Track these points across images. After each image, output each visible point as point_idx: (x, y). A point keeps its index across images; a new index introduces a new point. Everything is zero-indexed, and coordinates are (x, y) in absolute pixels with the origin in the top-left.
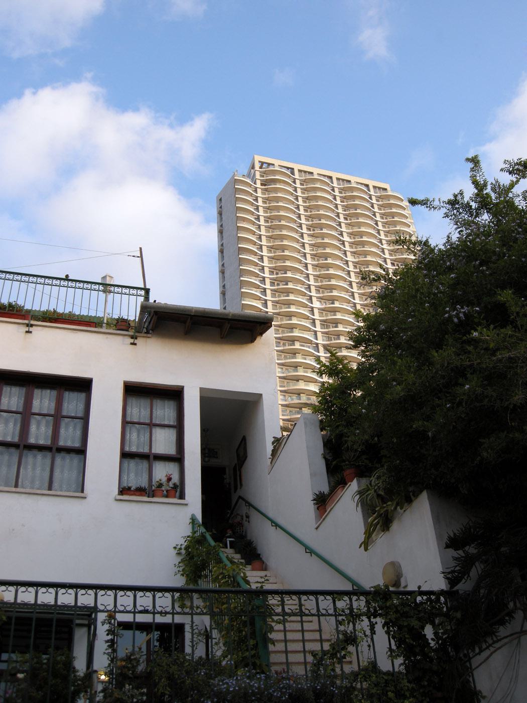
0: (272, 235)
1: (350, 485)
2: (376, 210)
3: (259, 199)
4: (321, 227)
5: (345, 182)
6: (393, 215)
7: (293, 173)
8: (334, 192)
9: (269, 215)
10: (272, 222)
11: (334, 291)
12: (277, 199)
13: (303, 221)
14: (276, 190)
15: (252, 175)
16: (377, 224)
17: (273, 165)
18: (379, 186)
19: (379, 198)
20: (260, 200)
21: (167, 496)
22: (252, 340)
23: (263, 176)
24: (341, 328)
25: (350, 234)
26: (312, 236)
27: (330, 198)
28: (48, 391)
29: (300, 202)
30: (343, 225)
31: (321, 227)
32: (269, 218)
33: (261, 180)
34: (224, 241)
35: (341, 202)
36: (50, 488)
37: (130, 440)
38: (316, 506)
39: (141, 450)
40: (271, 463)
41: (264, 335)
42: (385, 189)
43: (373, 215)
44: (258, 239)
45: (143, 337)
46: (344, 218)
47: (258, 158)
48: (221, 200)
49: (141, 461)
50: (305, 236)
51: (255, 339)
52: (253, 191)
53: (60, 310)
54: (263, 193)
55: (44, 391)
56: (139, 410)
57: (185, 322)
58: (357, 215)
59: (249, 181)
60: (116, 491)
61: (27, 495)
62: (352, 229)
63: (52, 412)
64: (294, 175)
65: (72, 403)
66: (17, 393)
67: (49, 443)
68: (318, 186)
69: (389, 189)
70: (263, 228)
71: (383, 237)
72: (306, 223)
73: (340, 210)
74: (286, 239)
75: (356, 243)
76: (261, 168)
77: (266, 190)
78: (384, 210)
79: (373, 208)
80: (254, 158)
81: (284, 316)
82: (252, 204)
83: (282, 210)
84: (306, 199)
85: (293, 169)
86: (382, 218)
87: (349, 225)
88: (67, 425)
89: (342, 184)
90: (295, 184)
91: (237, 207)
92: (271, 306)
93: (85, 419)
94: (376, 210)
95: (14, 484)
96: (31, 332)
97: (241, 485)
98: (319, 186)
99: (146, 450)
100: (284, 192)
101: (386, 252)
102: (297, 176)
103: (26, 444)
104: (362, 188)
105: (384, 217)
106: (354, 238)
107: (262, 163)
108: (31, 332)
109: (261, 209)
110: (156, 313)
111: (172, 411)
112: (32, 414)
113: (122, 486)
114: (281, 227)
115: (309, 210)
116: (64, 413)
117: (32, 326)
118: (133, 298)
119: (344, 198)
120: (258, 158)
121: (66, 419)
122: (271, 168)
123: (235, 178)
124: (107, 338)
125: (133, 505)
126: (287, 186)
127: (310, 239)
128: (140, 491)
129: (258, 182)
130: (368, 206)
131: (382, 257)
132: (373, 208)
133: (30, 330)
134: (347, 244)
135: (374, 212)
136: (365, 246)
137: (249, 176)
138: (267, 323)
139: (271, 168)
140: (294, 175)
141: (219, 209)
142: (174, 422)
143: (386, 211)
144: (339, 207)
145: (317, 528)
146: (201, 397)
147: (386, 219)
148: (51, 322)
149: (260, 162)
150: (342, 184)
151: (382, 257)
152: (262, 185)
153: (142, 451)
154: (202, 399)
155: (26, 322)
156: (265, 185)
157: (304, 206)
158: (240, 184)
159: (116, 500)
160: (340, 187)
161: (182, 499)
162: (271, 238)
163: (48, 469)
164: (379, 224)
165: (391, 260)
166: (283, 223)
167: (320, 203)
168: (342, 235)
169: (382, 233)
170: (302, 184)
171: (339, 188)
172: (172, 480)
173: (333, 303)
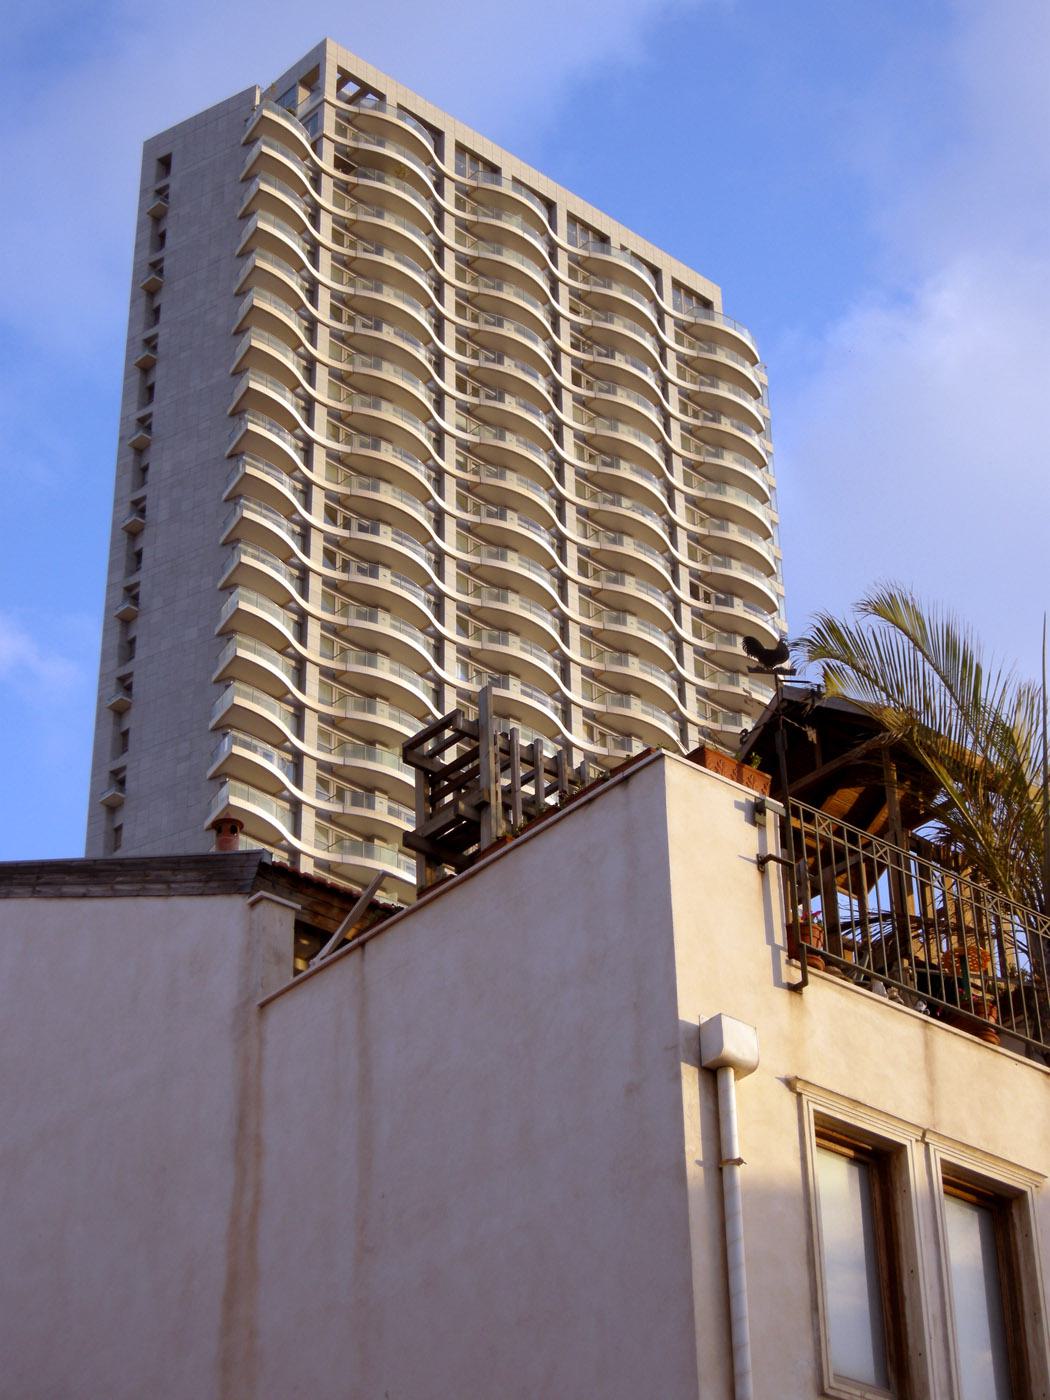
5: (467, 156)
17: (381, 97)
19: (466, 195)
24: (383, 716)
42: (706, 304)
48: (165, 163)
59: (302, 137)
69: (718, 306)
79: (318, 190)
81: (720, 666)
83: (392, 285)
127: (463, 421)
131: (297, 474)
132: (318, 190)
149: (341, 70)
151: (297, 474)
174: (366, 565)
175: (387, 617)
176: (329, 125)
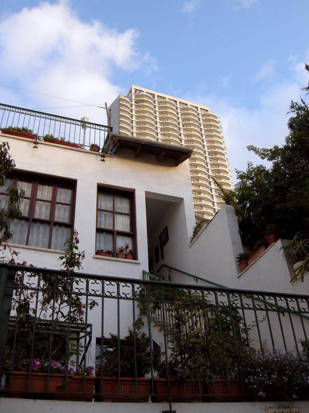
0: (140, 133)
1: (274, 244)
2: (201, 122)
3: (133, 111)
4: (169, 129)
6: (211, 126)
7: (154, 97)
8: (177, 110)
9: (138, 120)
10: (140, 125)
12: (144, 112)
13: (158, 126)
14: (144, 106)
15: (130, 97)
16: (201, 130)
17: (143, 91)
20: (134, 111)
21: (125, 258)
22: (177, 165)
23: (136, 98)
25: (185, 135)
26: (163, 135)
27: (175, 113)
28: (47, 187)
29: (157, 114)
30: (181, 130)
31: (169, 129)
32: (138, 122)
33: (135, 100)
35: (181, 116)
36: (49, 247)
37: (100, 221)
38: (238, 263)
39: (107, 228)
40: (191, 241)
41: (183, 163)
42: (207, 111)
43: (199, 125)
44: (131, 134)
45: (109, 157)
46: (182, 126)
47: (134, 87)
49: (108, 235)
50: (159, 134)
51: (179, 164)
52: (130, 106)
53: (55, 136)
54: (136, 108)
55: (44, 186)
56: (107, 203)
57: (135, 150)
58: (190, 125)
59: (128, 100)
60: (94, 252)
61: (35, 251)
62: (187, 132)
63: (50, 199)
64: (155, 98)
65: (64, 195)
66: (27, 186)
67: (48, 218)
68: (168, 105)
69: (209, 110)
70: (134, 128)
71: (204, 138)
72: (160, 127)
73: (180, 121)
74: (148, 136)
75: (188, 141)
76: (135, 92)
77: (138, 106)
78: (206, 122)
80: (131, 87)
82: (129, 114)
84: (161, 113)
85: (154, 95)
86: (204, 127)
87: (185, 130)
88: (59, 210)
89: (182, 105)
90: (155, 104)
91: (120, 114)
93: (72, 205)
94: (201, 122)
95: (25, 242)
96: (37, 147)
97: (163, 258)
98: (169, 106)
99: (111, 228)
100: (148, 107)
101: (206, 147)
102: (156, 99)
103: (33, 218)
104: (194, 109)
105: (206, 127)
106: (188, 138)
107: (136, 90)
108: (37, 147)
109: (134, 117)
110: (120, 141)
111: (126, 205)
112: (37, 200)
113: (97, 249)
114: (145, 128)
115: (162, 119)
116: (58, 201)
117: (38, 143)
118: (103, 132)
119: (183, 114)
120: (134, 87)
121: (58, 204)
122: (141, 93)
123: (120, 97)
124: (86, 155)
125: (105, 262)
127: (162, 136)
128: (109, 253)
129: (133, 101)
130: (197, 119)
131: (205, 162)
132: (200, 121)
133: (37, 146)
134: (183, 141)
135: (200, 123)
136: (194, 143)
137: (128, 97)
138: (188, 153)
139: (141, 93)
140: (155, 98)
141: (109, 115)
142: (128, 211)
143: (207, 123)
144: (180, 119)
145: (238, 277)
146: (146, 198)
147: (207, 128)
148: (50, 142)
149: (135, 89)
150: (182, 105)
152: (135, 102)
153: (108, 228)
154: (147, 199)
155: (34, 140)
156: (137, 103)
157: (159, 117)
158: (123, 101)
159: (94, 258)
160: (181, 107)
161: (136, 260)
162: (139, 134)
163: (47, 236)
164: (203, 130)
165: (208, 152)
166: (146, 126)
167: (169, 116)
168: (180, 135)
169: (204, 136)
170: (159, 104)
171: (180, 108)
172: (129, 248)
174: (218, 173)
175: (223, 179)
176: (133, 97)
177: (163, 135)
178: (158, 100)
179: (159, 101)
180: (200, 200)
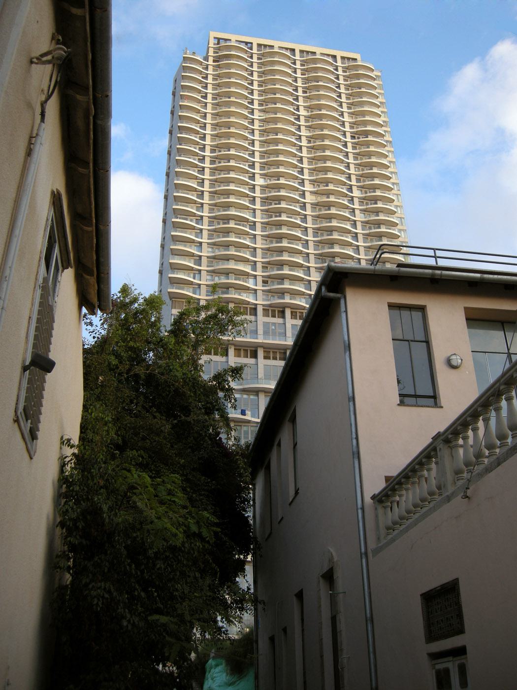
3: (342, 95)
11: (328, 173)
18: (348, 56)
20: (343, 96)
25: (307, 108)
34: (173, 122)
77: (218, 66)
92: (358, 202)
100: (237, 68)
120: (213, 34)
122: (228, 44)
126: (329, 74)
136: (323, 120)
139: (228, 44)
170: (344, 71)
173: (327, 186)
177: (264, 111)
178: (342, 64)
179: (345, 65)
180: (330, 246)
